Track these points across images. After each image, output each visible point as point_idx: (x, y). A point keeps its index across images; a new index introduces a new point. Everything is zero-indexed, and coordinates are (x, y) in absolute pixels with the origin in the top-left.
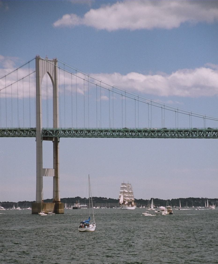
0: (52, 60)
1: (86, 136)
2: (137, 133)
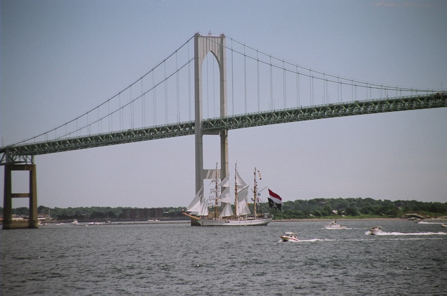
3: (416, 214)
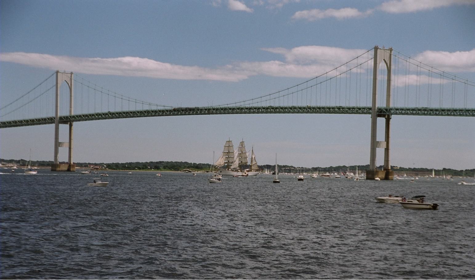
0: (388, 49)
1: (357, 113)
2: (417, 111)
3: (188, 170)
